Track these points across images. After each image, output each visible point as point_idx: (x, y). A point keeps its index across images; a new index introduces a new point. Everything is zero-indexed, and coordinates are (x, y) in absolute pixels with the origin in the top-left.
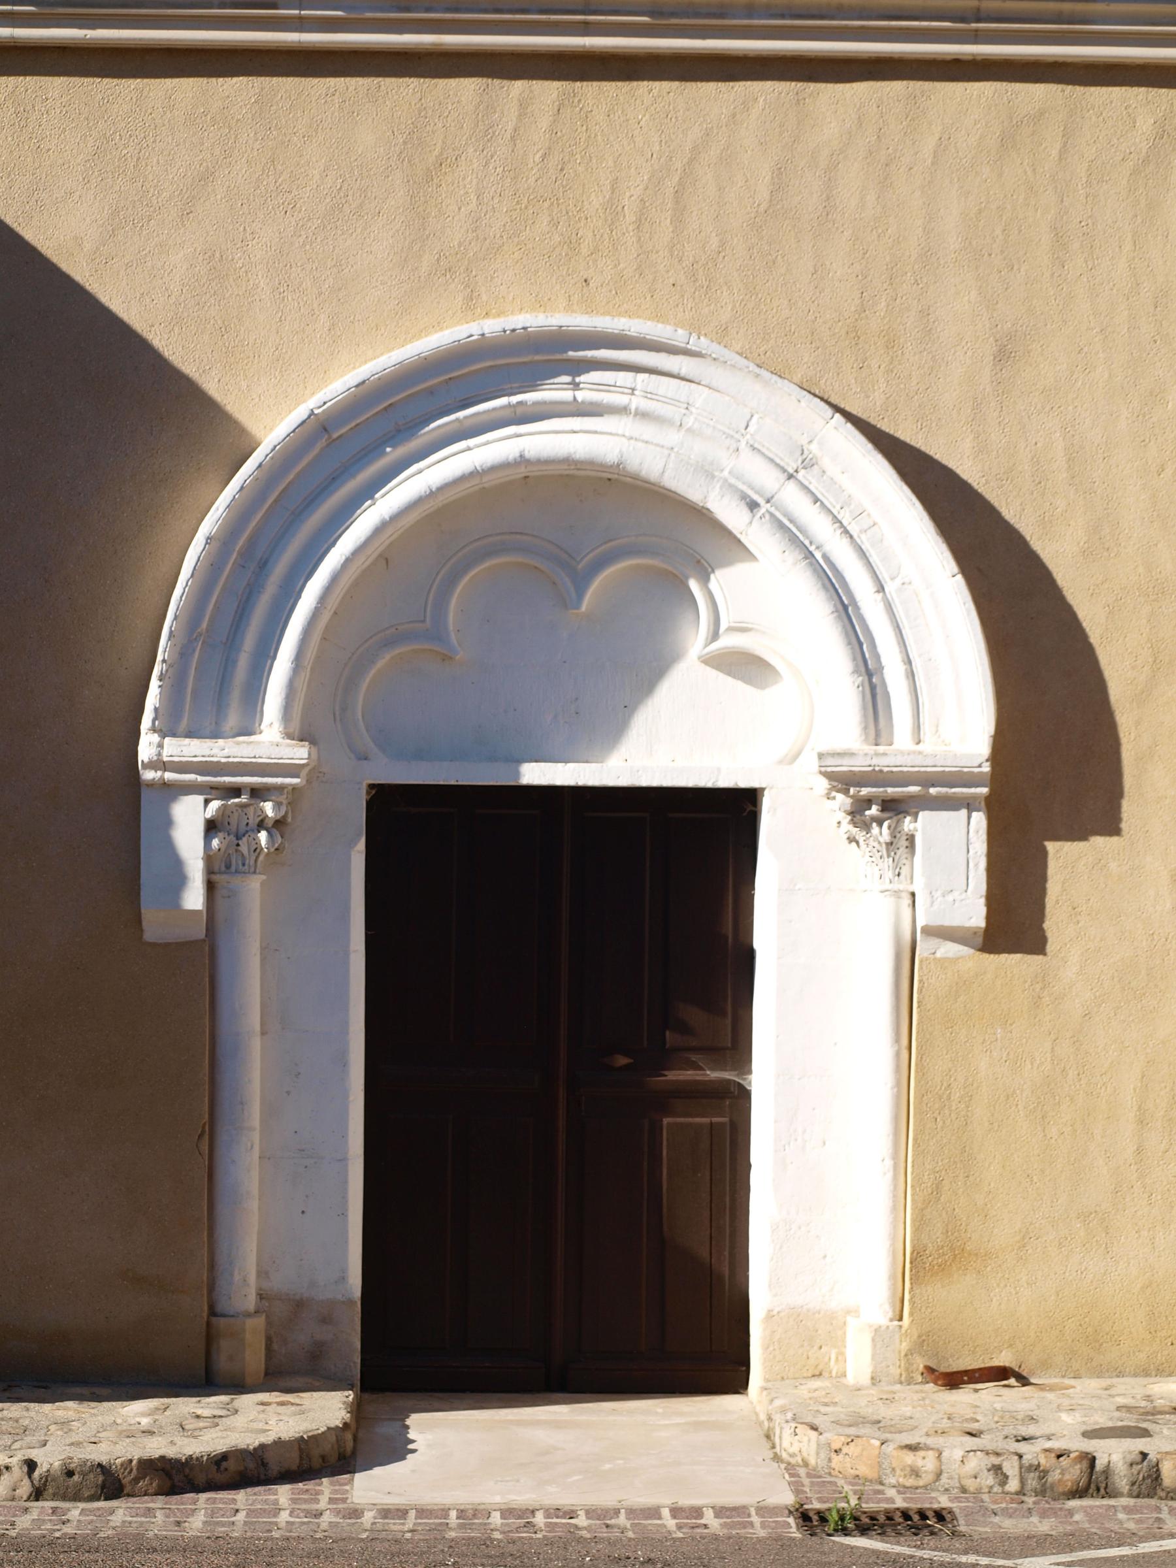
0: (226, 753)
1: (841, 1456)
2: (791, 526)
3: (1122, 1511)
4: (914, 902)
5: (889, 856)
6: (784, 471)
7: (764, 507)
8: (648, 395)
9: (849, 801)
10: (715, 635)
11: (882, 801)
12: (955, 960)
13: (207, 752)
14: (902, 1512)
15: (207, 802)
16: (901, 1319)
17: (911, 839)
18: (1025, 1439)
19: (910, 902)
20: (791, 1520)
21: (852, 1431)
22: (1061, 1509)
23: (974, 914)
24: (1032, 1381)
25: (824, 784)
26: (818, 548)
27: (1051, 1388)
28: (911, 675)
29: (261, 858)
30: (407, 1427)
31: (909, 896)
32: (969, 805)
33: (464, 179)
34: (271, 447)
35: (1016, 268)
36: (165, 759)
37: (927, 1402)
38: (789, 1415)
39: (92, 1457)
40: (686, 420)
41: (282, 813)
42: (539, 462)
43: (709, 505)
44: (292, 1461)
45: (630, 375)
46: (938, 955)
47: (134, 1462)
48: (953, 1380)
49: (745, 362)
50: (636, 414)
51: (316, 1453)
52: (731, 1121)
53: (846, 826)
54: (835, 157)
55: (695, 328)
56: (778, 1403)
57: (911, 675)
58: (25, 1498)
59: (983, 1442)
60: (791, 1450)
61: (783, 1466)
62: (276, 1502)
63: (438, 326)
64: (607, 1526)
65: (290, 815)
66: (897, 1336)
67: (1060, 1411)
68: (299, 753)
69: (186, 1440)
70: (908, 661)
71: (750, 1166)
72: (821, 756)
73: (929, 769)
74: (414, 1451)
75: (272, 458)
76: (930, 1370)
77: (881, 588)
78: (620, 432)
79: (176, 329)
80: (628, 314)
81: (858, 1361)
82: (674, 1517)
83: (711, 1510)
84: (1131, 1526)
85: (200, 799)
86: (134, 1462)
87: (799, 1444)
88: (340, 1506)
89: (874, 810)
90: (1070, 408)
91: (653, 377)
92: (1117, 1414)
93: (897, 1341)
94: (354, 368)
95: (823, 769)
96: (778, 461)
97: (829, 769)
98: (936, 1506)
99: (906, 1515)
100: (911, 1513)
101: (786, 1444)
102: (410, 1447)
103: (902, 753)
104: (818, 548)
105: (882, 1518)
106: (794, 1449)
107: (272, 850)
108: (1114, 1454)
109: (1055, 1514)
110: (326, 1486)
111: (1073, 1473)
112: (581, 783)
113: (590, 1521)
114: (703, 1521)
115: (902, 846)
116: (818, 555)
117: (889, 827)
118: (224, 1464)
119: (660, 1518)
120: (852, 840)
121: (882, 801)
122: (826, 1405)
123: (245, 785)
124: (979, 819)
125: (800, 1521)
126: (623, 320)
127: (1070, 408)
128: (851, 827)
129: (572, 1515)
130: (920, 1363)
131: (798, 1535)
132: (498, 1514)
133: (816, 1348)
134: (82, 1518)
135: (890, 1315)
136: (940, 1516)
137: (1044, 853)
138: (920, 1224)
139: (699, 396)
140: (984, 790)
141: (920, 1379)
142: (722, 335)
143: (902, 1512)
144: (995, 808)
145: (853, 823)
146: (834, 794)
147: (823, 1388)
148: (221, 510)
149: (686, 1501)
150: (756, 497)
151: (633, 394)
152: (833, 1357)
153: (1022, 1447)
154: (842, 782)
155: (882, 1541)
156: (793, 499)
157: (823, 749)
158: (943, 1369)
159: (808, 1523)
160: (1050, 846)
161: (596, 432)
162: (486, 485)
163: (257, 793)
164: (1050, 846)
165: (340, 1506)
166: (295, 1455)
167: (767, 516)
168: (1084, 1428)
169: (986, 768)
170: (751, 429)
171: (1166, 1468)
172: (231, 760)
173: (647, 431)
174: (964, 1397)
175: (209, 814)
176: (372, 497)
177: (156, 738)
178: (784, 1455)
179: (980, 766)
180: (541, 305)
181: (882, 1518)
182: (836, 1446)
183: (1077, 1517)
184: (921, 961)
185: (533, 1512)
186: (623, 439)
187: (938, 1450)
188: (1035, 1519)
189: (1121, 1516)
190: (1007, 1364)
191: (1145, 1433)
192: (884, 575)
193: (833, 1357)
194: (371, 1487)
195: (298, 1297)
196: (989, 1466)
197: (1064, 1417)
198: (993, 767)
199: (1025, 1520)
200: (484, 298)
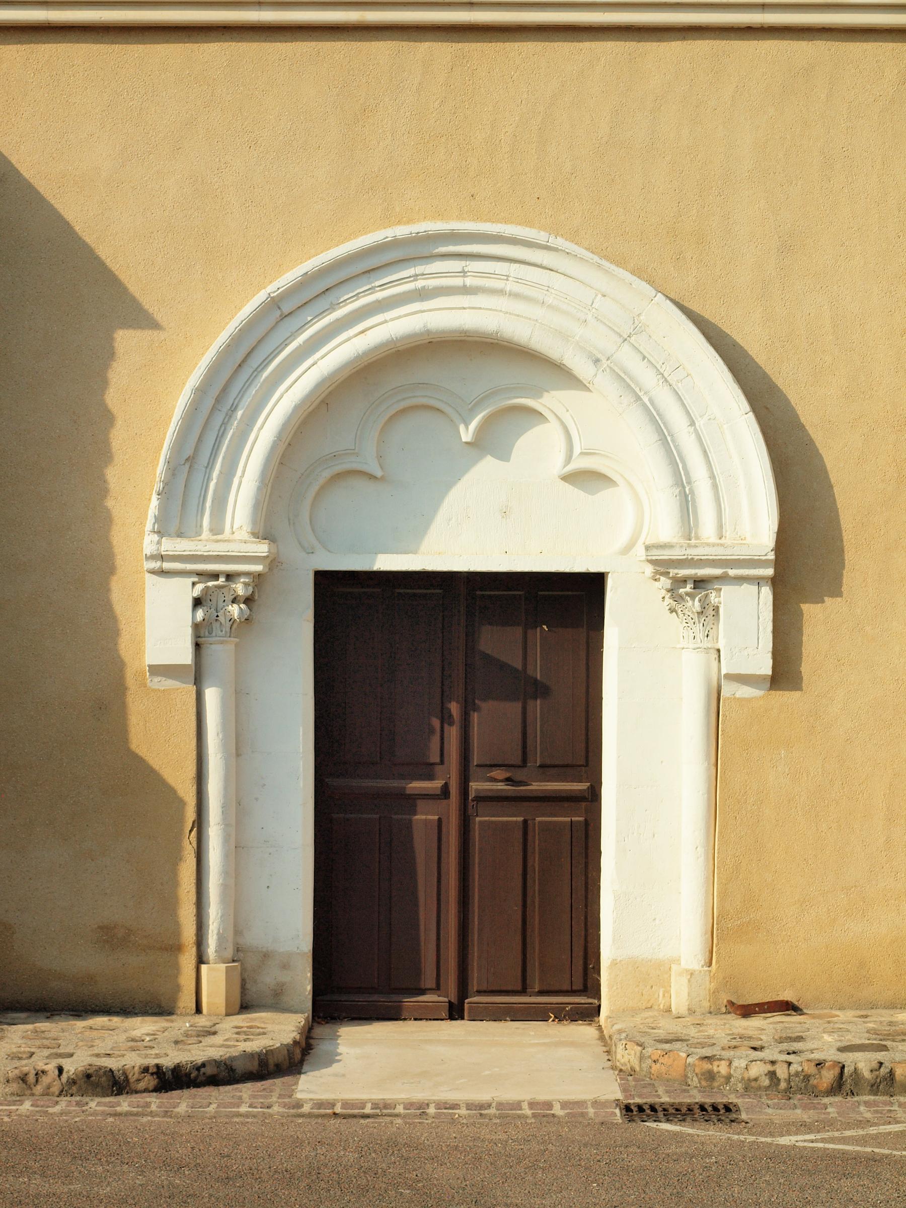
0: (207, 548)
1: (658, 1065)
2: (625, 377)
3: (864, 1105)
4: (719, 656)
5: (699, 622)
6: (621, 336)
7: (605, 363)
8: (518, 280)
9: (669, 582)
10: (569, 459)
11: (692, 584)
12: (749, 700)
13: (194, 548)
14: (650, 1106)
15: (194, 584)
16: (710, 965)
17: (716, 609)
18: (794, 1053)
19: (717, 656)
20: (617, 1111)
21: (667, 1046)
22: (819, 1103)
23: (765, 667)
24: (805, 1011)
25: (649, 569)
26: (645, 393)
27: (819, 1017)
28: (715, 486)
29: (235, 626)
30: (338, 1044)
31: (716, 652)
32: (758, 581)
33: (382, 121)
34: (239, 322)
35: (794, 182)
36: (163, 553)
37: (727, 1026)
38: (624, 1035)
39: (106, 1065)
40: (540, 292)
41: (250, 592)
42: (437, 332)
43: (564, 362)
44: (254, 1066)
45: (506, 265)
46: (737, 696)
47: (136, 1068)
48: (747, 1011)
49: (591, 255)
50: (510, 295)
51: (271, 1062)
52: (586, 820)
53: (668, 601)
54: (658, 101)
55: (555, 231)
56: (616, 1027)
57: (715, 486)
58: (57, 1093)
59: (766, 1054)
60: (622, 1061)
61: (616, 1072)
62: (240, 1098)
63: (364, 231)
64: (481, 1115)
65: (256, 594)
66: (708, 978)
67: (824, 1032)
68: (262, 549)
69: (176, 1053)
70: (713, 477)
71: (600, 852)
72: (648, 548)
73: (728, 557)
74: (339, 1061)
75: (240, 330)
76: (731, 1003)
77: (692, 424)
78: (499, 308)
79: (170, 234)
80: (506, 221)
81: (680, 996)
82: (531, 1108)
83: (558, 1104)
84: (868, 1115)
85: (189, 581)
86: (136, 1068)
87: (626, 1056)
88: (286, 1100)
89: (689, 588)
90: (835, 287)
91: (522, 266)
92: (867, 1035)
93: (708, 983)
94: (301, 263)
95: (649, 558)
96: (616, 329)
97: (654, 558)
98: (725, 1100)
99: (702, 1108)
100: (706, 1106)
101: (619, 1057)
102: (337, 1058)
103: (708, 545)
104: (645, 393)
105: (684, 1110)
106: (625, 1060)
107: (243, 620)
108: (863, 1062)
109: (815, 1108)
110: (277, 1084)
111: (828, 1076)
112: (472, 569)
113: (469, 1112)
114: (552, 1112)
115: (709, 613)
116: (646, 399)
117: (700, 600)
118: (203, 1070)
119: (521, 1109)
120: (672, 610)
121: (692, 584)
122: (653, 1029)
123: (222, 572)
124: (767, 593)
125: (624, 1112)
126: (500, 225)
127: (835, 287)
128: (671, 601)
129: (455, 1106)
130: (724, 998)
131: (620, 1121)
132: (402, 1106)
133: (648, 987)
134: (97, 1108)
135: (702, 963)
136: (727, 1109)
137: (801, 614)
138: (723, 895)
139: (557, 281)
140: (770, 572)
141: (724, 1010)
142: (574, 236)
143: (650, 1106)
144: (776, 582)
145: (672, 597)
146: (658, 576)
147: (651, 1017)
148: (203, 369)
149: (542, 1097)
150: (599, 356)
151: (507, 280)
152: (661, 995)
153: (791, 1058)
154: (662, 567)
155: (680, 1125)
156: (627, 357)
157: (649, 542)
158: (741, 1003)
159: (630, 1113)
160: (805, 607)
161: (480, 308)
162: (399, 349)
163: (229, 577)
164: (805, 607)
165: (286, 1100)
166: (256, 1063)
167: (608, 370)
168: (839, 1044)
169: (772, 556)
170: (595, 305)
171: (899, 1072)
172: (211, 553)
173: (519, 307)
174: (755, 1023)
175: (195, 595)
176: (692, 559)
177: (156, 537)
178: (618, 1064)
179: (766, 555)
180: (440, 215)
181: (684, 1110)
182: (655, 1058)
183: (830, 1110)
184: (724, 700)
185: (428, 1105)
186: (501, 314)
187: (729, 1060)
188: (798, 1111)
189: (862, 1108)
190: (789, 999)
191: (885, 1048)
192: (695, 414)
193: (661, 995)
194: (311, 1086)
195: (264, 950)
196: (766, 1072)
197: (826, 1037)
198: (776, 554)
199: (791, 1111)
200: (398, 209)
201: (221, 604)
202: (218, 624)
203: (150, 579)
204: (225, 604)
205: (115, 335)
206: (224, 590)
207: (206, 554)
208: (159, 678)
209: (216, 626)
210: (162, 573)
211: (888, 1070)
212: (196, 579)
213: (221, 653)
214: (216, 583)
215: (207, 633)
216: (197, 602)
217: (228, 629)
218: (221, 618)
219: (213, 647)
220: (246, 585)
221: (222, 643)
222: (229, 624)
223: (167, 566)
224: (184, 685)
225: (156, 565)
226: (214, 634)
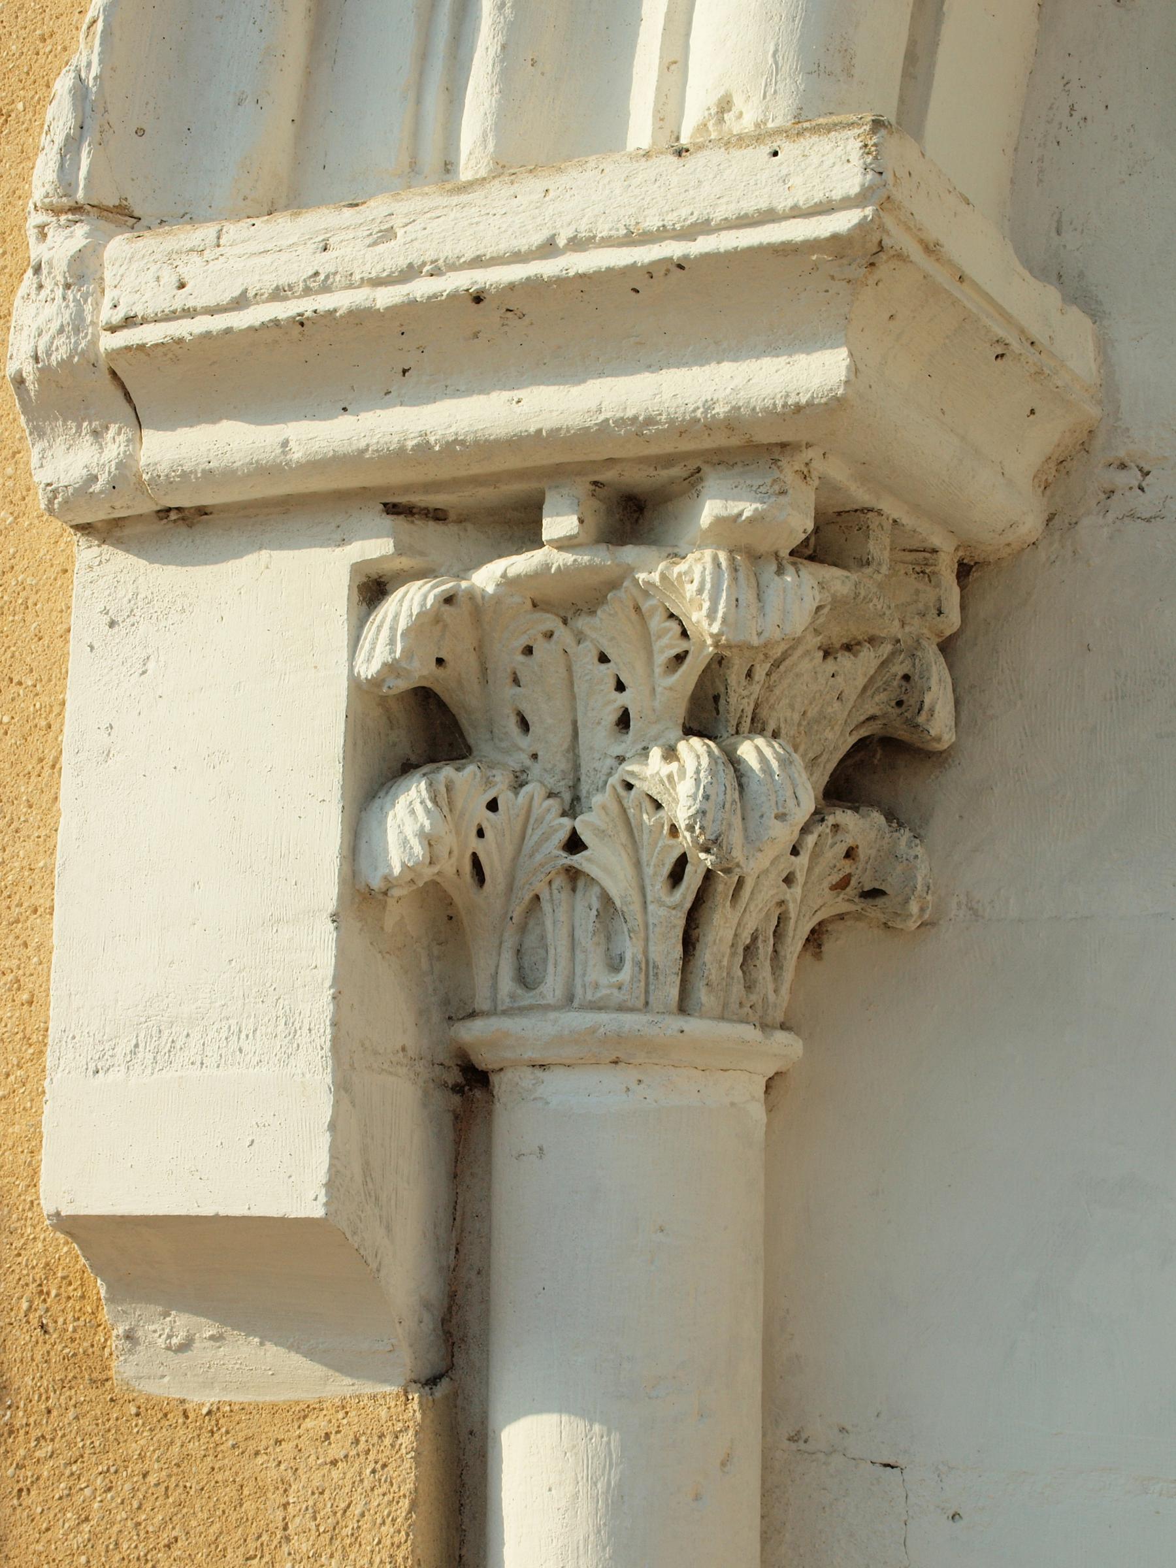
13: (297, 266)
15: (373, 589)
85: (323, 569)
172: (422, 288)
175: (368, 669)
201: (598, 737)
202: (586, 905)
203: (106, 577)
204: (627, 744)
205: (839, 197)
206: (603, 628)
207: (385, 297)
208: (181, 1323)
209: (566, 920)
210: (179, 522)
211: (845, 817)
212: (376, 547)
213: (635, 1138)
214: (521, 563)
215: (507, 984)
216: (420, 727)
217: (668, 951)
218: (605, 861)
219: (559, 1088)
220: (749, 555)
221: (617, 1055)
222: (669, 909)
223: (180, 450)
224: (342, 1386)
225: (72, 459)
226: (552, 987)
